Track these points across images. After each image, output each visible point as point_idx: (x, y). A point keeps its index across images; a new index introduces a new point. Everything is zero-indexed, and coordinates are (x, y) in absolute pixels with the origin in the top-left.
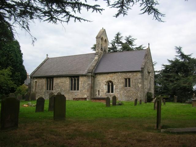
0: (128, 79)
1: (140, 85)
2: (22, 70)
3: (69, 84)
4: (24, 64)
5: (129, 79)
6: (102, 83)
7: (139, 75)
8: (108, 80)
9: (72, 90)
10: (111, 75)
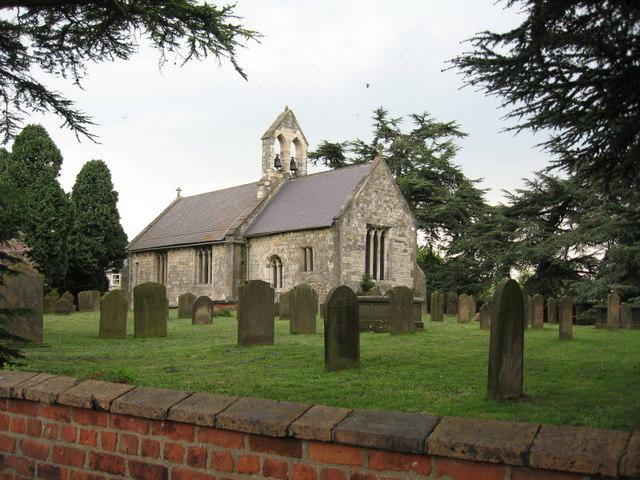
1: (331, 266)
2: (119, 233)
4: (121, 222)
5: (311, 249)
6: (260, 252)
7: (329, 235)
8: (271, 253)
10: (276, 239)
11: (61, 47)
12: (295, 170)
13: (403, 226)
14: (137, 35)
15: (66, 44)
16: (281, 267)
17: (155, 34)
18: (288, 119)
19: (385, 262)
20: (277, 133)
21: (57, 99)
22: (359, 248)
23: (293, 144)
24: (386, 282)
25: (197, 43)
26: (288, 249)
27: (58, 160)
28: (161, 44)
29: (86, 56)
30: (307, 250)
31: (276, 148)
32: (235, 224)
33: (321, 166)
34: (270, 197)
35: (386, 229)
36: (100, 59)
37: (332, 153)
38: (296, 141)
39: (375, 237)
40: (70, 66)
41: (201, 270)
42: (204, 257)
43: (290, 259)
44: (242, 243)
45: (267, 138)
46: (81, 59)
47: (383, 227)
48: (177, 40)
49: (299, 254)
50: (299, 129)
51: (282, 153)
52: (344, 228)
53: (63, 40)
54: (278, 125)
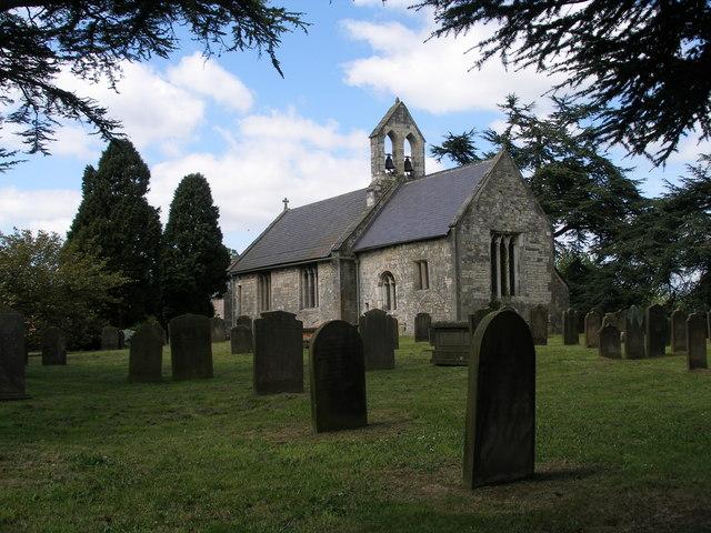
0: (422, 265)
3: (301, 290)
5: (426, 263)
6: (371, 269)
7: (445, 251)
8: (383, 269)
9: (307, 306)
10: (388, 254)
11: (91, 48)
12: (411, 171)
13: (536, 230)
14: (179, 28)
15: (97, 44)
16: (394, 285)
17: (196, 24)
18: (400, 113)
19: (516, 274)
20: (387, 129)
21: (90, 106)
22: (482, 260)
23: (406, 141)
24: (521, 298)
25: (243, 33)
26: (399, 263)
27: (144, 174)
28: (204, 34)
29: (122, 56)
30: (421, 264)
31: (388, 147)
32: (341, 238)
33: (448, 163)
34: (381, 204)
35: (514, 235)
36: (137, 59)
37: (458, 147)
38: (410, 137)
39: (503, 245)
40: (105, 69)
41: (307, 292)
42: (309, 277)
43: (404, 275)
44: (349, 260)
45: (377, 136)
46: (116, 61)
47: (511, 233)
48: (222, 29)
49: (411, 270)
50: (413, 123)
51: (394, 152)
52: (463, 237)
53: (93, 40)
54: (389, 120)
